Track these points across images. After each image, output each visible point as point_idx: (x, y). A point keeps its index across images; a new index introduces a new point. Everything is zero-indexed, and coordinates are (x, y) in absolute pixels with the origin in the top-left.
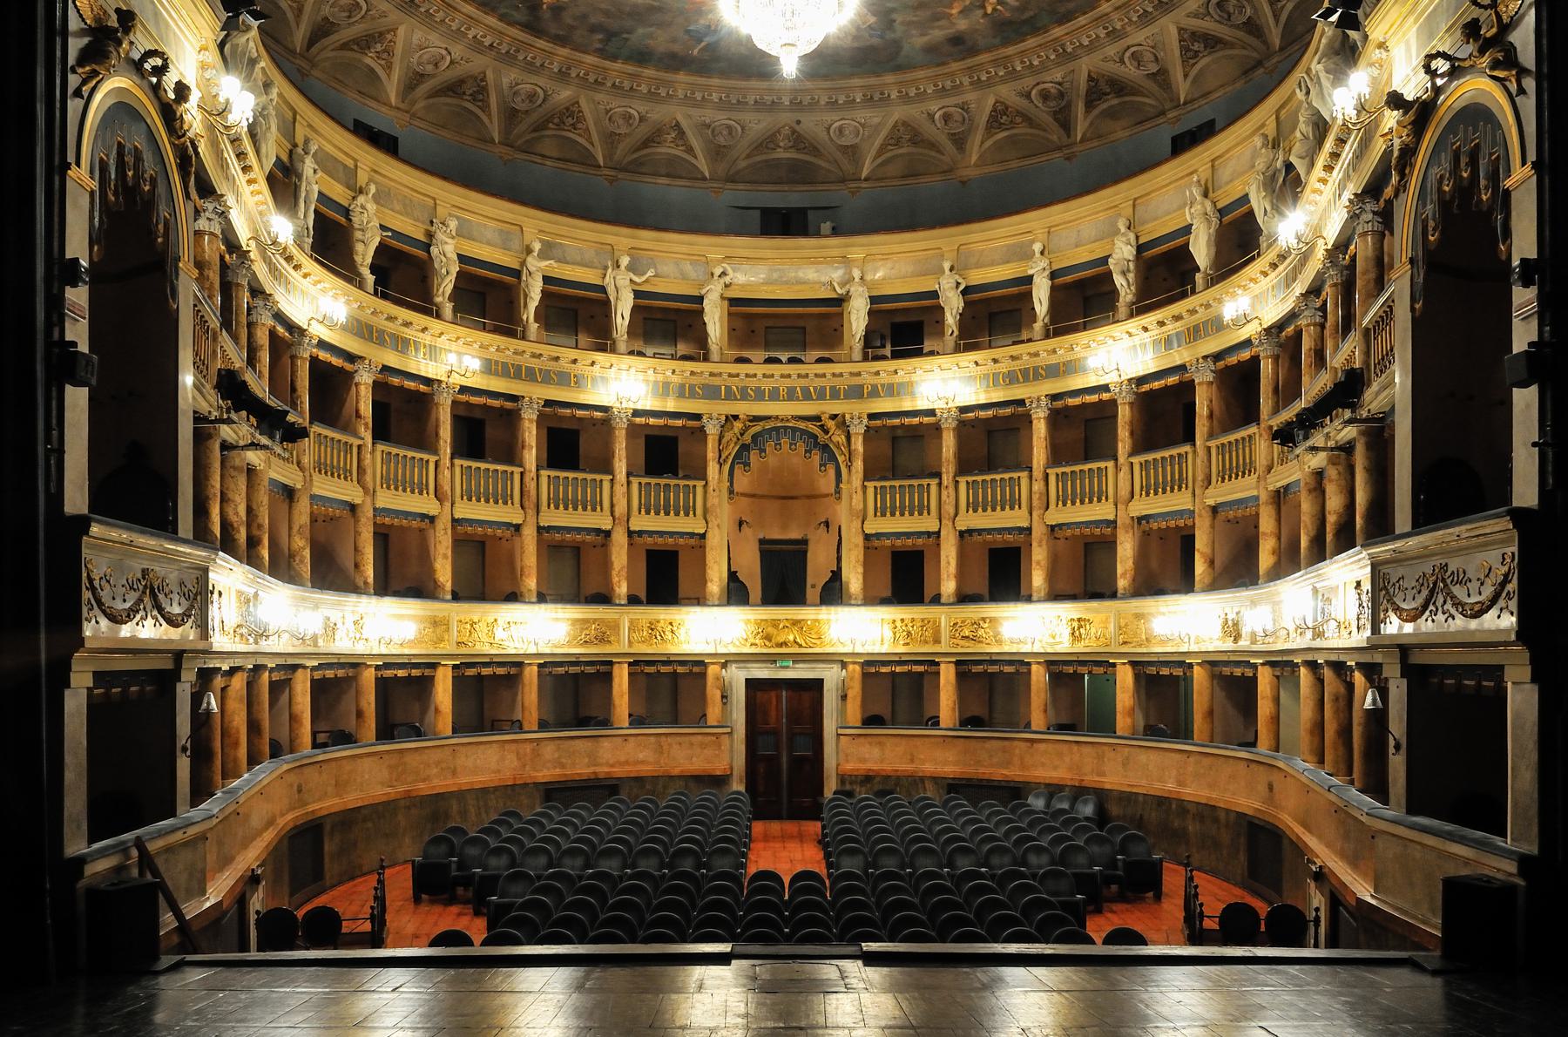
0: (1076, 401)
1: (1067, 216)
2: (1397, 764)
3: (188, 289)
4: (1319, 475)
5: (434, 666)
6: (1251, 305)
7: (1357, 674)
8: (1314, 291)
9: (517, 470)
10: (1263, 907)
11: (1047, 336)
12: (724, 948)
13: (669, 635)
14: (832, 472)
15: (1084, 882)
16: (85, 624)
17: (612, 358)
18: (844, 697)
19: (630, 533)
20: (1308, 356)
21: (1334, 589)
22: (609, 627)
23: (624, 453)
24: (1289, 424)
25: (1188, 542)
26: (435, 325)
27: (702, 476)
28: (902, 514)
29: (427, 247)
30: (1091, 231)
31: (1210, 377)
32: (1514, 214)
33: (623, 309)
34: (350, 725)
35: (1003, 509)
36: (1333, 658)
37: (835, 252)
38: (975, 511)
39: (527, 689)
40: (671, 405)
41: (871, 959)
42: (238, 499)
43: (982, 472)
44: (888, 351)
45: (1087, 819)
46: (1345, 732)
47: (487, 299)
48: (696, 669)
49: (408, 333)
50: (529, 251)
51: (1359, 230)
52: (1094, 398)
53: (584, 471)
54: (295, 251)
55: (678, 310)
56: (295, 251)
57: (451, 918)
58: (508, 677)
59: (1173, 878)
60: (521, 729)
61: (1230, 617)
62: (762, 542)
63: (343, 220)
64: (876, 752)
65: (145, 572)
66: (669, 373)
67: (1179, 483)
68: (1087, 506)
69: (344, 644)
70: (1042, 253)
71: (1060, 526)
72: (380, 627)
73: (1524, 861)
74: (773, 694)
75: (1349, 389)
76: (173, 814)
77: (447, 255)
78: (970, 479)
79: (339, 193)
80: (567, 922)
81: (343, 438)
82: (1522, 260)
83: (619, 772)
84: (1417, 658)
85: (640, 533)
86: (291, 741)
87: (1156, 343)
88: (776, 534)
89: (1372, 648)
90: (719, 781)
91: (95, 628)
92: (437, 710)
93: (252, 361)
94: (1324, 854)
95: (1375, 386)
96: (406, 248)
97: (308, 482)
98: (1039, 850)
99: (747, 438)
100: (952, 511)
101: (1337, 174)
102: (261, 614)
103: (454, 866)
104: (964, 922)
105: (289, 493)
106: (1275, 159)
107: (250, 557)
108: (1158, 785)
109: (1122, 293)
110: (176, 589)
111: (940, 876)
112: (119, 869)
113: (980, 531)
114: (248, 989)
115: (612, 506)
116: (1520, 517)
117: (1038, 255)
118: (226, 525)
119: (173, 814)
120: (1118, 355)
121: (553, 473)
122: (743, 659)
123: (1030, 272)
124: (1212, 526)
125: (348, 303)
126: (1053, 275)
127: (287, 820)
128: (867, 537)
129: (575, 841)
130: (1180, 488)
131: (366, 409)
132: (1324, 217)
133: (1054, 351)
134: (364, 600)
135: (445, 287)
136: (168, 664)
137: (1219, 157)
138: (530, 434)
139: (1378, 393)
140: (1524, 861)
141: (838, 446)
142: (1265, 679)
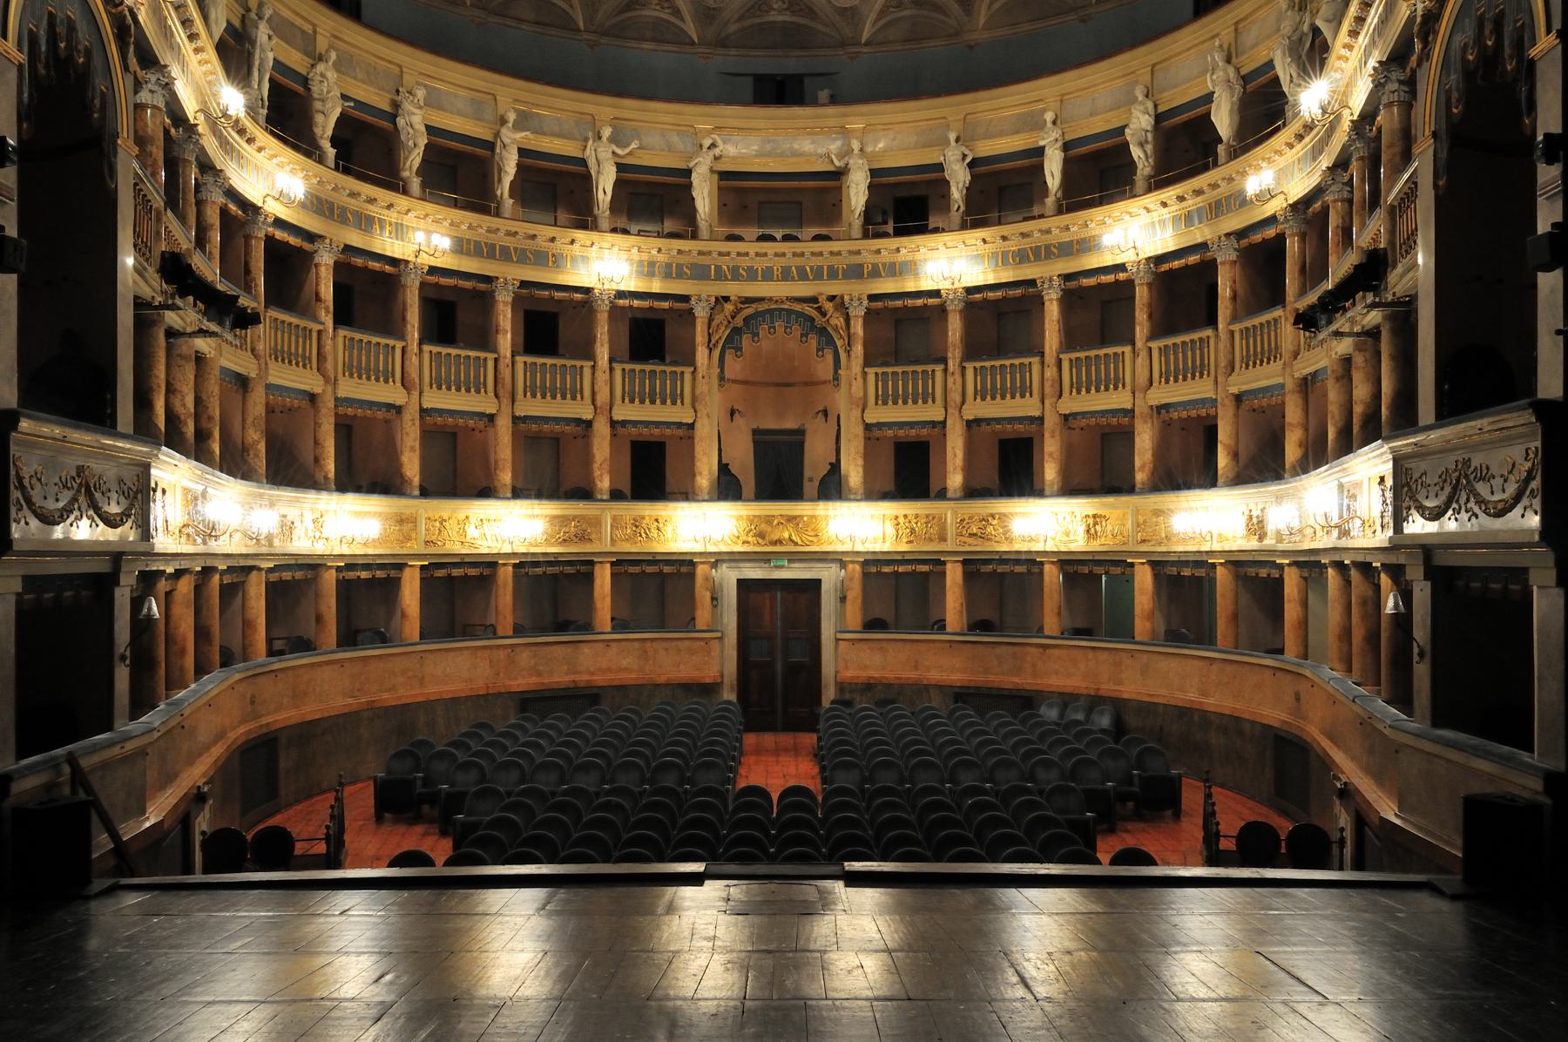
0: (1091, 281)
1: (1083, 82)
2: (1422, 672)
3: (127, 165)
4: (1347, 361)
5: (400, 567)
6: (1276, 178)
7: (1383, 576)
8: (1341, 164)
9: (491, 356)
10: (1285, 827)
11: (1060, 211)
12: (697, 867)
13: (654, 533)
14: (829, 358)
15: (1094, 798)
16: (14, 526)
17: (594, 236)
18: (843, 599)
19: (613, 424)
20: (1335, 234)
21: (1358, 485)
22: (590, 525)
23: (606, 338)
24: (1312, 307)
25: (1210, 434)
26: (402, 202)
27: (691, 362)
28: (905, 403)
29: (393, 117)
30: (1111, 97)
31: (1233, 256)
32: (1539, 85)
33: (605, 183)
34: (309, 630)
35: (1013, 397)
36: (1360, 558)
37: (832, 122)
38: (984, 399)
39: (501, 591)
40: (656, 286)
41: (855, 880)
42: (185, 389)
43: (991, 357)
44: (890, 228)
45: (1103, 731)
46: (1373, 638)
47: (458, 174)
48: (684, 569)
49: (373, 210)
50: (503, 121)
51: (1385, 100)
52: (1110, 278)
53: (563, 356)
54: (248, 123)
55: (648, 183)
56: (248, 123)
57: (413, 838)
58: (481, 578)
59: (1192, 796)
60: (495, 636)
61: (1254, 514)
62: (755, 432)
63: (300, 89)
64: (878, 658)
65: (80, 470)
66: (654, 252)
67: (1199, 370)
68: (1103, 394)
69: (303, 544)
70: (1054, 123)
71: (1074, 415)
72: (340, 525)
73: (1550, 778)
74: (767, 595)
75: (1372, 271)
76: (109, 727)
77: (414, 125)
78: (978, 365)
79: (295, 60)
80: (536, 841)
81: (302, 323)
82: (1547, 136)
83: (600, 679)
84: (1442, 560)
85: (624, 423)
86: (245, 648)
87: (1176, 219)
88: (770, 424)
89: (1394, 547)
90: (708, 689)
91: (24, 529)
92: (404, 615)
93: (201, 242)
94: (1349, 769)
95: (1400, 269)
96: (370, 119)
97: (263, 370)
98: (1048, 764)
99: (739, 321)
100: (958, 399)
101: (1363, 40)
102: (204, 511)
103: (419, 783)
104: (964, 841)
105: (242, 382)
106: (1301, 22)
107: (198, 452)
108: (1180, 695)
109: (1140, 166)
110: (114, 487)
111: (984, 792)
112: (50, 787)
113: (988, 421)
114: (185, 914)
115: (593, 394)
116: (1544, 410)
117: (1049, 125)
118: (171, 417)
119: (109, 727)
120: (1135, 232)
121: (530, 359)
122: (734, 558)
123: (1042, 143)
124: (1236, 416)
125: (306, 178)
126: (1066, 147)
127: (239, 733)
128: (868, 427)
129: (551, 754)
130: (1201, 376)
131: (327, 291)
132: (1350, 85)
133: (1067, 228)
134: (324, 496)
135: (413, 160)
136: (102, 566)
137: (1246, 18)
138: (505, 318)
139: (1402, 276)
140: (1550, 778)
141: (836, 329)
142: (1292, 581)
